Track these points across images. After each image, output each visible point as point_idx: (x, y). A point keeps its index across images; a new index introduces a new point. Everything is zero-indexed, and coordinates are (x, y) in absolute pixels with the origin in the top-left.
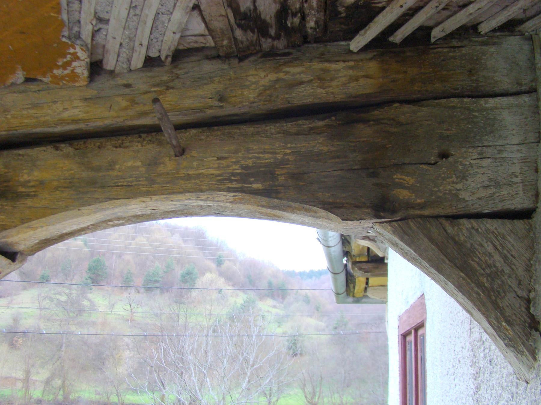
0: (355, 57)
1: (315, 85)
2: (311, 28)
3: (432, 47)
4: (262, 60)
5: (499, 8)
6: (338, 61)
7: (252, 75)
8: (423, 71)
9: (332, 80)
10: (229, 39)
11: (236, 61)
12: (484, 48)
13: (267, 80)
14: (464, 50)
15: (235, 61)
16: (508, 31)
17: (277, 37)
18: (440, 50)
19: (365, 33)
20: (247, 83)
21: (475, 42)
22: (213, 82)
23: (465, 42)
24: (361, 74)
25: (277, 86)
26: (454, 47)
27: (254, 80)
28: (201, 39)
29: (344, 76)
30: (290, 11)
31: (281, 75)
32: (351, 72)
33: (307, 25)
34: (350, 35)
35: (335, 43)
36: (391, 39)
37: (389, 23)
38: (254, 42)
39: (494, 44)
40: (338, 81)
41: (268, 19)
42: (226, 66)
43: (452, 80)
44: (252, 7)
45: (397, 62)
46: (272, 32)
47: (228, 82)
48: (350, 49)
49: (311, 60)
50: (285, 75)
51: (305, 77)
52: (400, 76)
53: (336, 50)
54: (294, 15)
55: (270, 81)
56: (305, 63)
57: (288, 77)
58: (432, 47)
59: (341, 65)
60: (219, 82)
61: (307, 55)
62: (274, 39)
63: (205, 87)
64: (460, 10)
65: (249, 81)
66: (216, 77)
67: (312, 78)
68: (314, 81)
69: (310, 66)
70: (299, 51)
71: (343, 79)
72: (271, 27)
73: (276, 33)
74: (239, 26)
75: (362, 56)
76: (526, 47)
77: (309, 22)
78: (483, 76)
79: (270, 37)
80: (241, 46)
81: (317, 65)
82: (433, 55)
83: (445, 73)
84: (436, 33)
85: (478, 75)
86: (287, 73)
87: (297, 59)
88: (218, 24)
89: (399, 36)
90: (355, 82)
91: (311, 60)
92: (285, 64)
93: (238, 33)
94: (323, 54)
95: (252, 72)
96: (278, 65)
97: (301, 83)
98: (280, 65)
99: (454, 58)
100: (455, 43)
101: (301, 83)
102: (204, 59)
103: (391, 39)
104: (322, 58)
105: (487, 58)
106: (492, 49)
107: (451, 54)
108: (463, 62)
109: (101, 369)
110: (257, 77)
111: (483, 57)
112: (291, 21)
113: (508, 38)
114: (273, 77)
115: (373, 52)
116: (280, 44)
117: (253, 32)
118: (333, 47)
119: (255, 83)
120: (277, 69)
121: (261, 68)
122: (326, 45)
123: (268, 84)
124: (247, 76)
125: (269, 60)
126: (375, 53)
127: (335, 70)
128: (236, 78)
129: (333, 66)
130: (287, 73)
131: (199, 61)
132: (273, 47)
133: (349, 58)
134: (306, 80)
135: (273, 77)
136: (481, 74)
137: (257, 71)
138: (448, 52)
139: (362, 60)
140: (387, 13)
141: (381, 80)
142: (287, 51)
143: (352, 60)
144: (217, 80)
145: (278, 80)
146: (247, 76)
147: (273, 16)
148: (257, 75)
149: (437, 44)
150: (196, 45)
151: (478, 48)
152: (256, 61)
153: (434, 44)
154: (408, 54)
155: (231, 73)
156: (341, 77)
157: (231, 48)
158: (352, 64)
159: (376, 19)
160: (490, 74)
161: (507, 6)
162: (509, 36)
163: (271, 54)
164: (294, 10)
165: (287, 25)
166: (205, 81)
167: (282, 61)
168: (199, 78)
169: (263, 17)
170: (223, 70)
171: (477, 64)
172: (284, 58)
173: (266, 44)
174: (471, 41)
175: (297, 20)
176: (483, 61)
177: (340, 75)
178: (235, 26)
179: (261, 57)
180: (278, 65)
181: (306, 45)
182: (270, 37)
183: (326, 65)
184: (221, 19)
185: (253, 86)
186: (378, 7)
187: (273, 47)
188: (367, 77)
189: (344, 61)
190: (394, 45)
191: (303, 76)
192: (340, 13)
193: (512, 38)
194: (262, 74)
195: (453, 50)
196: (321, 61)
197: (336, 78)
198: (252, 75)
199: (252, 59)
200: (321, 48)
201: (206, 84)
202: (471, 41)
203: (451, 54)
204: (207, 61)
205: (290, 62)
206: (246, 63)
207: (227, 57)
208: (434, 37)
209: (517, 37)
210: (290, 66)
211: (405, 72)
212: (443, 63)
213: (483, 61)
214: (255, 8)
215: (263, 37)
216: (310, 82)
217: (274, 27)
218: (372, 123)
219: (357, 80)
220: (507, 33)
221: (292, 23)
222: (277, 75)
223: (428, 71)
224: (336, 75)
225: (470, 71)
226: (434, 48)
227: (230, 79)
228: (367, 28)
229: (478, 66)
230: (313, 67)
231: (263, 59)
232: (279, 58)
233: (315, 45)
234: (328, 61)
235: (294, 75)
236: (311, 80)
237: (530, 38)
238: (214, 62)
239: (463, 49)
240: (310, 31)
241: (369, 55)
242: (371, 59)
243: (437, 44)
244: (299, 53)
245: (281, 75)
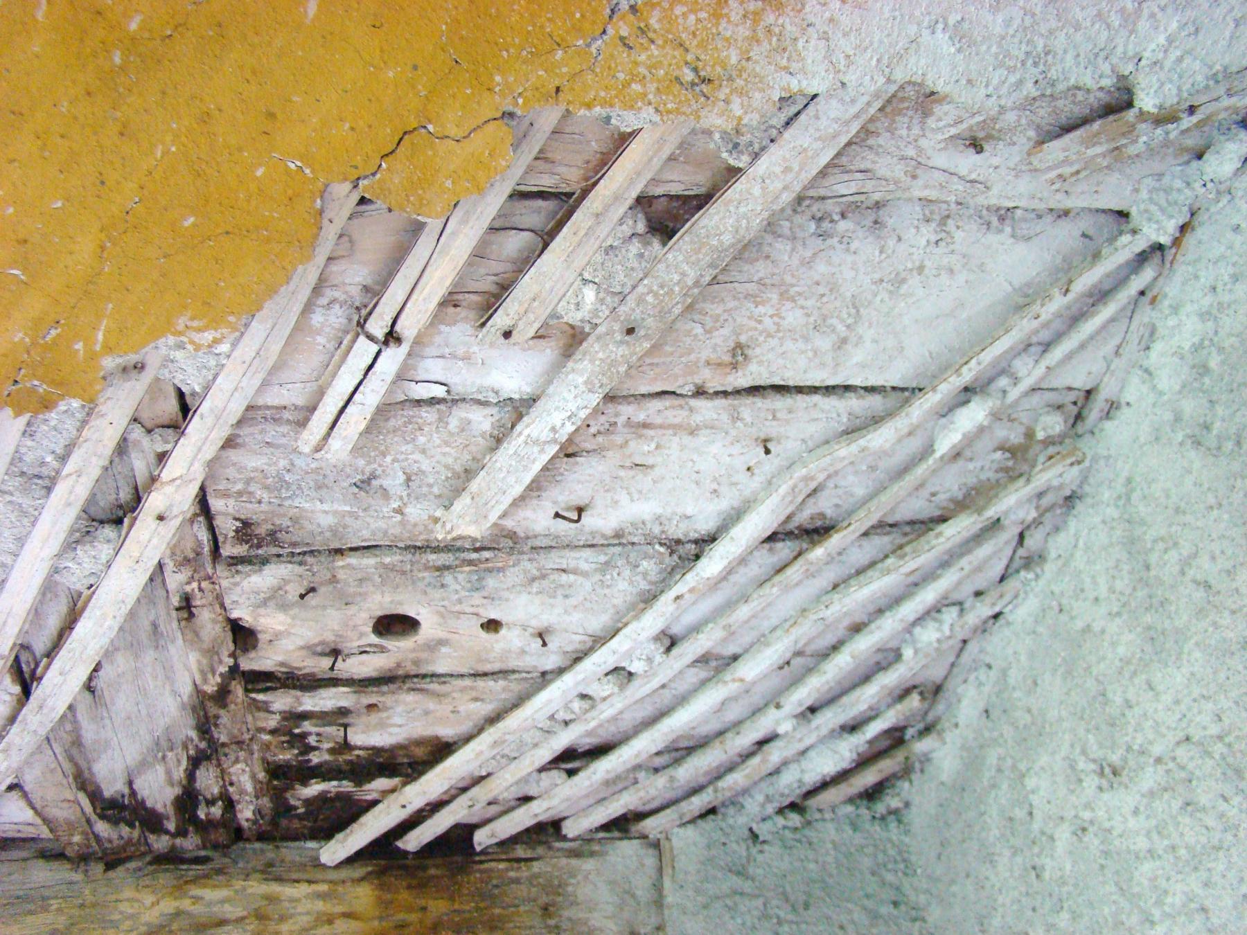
0: (334, 875)
1: (248, 928)
2: (247, 820)
3: (477, 858)
4: (151, 868)
5: (592, 801)
6: (297, 881)
7: (128, 900)
8: (456, 906)
9: (282, 919)
10: (84, 833)
11: (100, 867)
12: (574, 862)
13: (156, 912)
14: (536, 867)
15: (97, 869)
16: (620, 830)
17: (181, 832)
18: (493, 864)
19: (345, 839)
20: (116, 917)
21: (559, 850)
22: (45, 909)
23: (540, 850)
24: (340, 909)
25: (175, 927)
26: (518, 860)
27: (130, 911)
28: (31, 829)
29: (308, 913)
30: (201, 798)
31: (186, 904)
32: (320, 905)
33: (239, 816)
34: (327, 833)
35: (297, 844)
36: (400, 844)
37: (386, 829)
38: (135, 840)
39: (592, 854)
40: (295, 923)
41: (159, 808)
42: (78, 876)
43: (511, 925)
44: (126, 791)
45: (409, 887)
46: (171, 826)
47: (76, 912)
48: (318, 859)
49: (247, 877)
50: (194, 904)
51: (231, 911)
52: (413, 917)
53: (298, 858)
54: (211, 802)
55: (161, 915)
56: (234, 882)
57: (197, 909)
58: (477, 858)
59: (304, 889)
60: (59, 910)
61: (241, 865)
62: (174, 836)
63: (30, 919)
64: (519, 806)
65: (121, 913)
66: (56, 897)
67: (245, 913)
68: (247, 921)
69: (244, 889)
70: (225, 855)
71: (305, 918)
72: (168, 819)
73: (177, 827)
74: (102, 817)
75: (345, 873)
76: (650, 861)
77: (241, 811)
78: (570, 919)
79: (167, 832)
80: (107, 845)
81: (257, 887)
82: (478, 875)
83: (497, 911)
84: (481, 838)
85: (560, 916)
86: (197, 899)
87: (220, 871)
88: (60, 813)
89: (413, 841)
90: (327, 927)
91: (247, 875)
92: (194, 881)
93: (102, 828)
94: (271, 864)
95: (128, 893)
96: (181, 882)
97: (222, 923)
98: (186, 882)
99: (517, 881)
100: (520, 851)
101: (222, 923)
102: (36, 857)
103: (400, 844)
104: (269, 872)
105: (578, 883)
106: (589, 865)
107: (512, 874)
108: (534, 890)
109: (1196, 869)
110: (136, 905)
111: (573, 881)
112: (206, 810)
113: (618, 843)
114: (168, 906)
115: (367, 865)
116: (190, 843)
117: (131, 825)
118: (292, 852)
119: (131, 917)
120: (179, 889)
121: (147, 886)
122: (277, 847)
123: (156, 922)
124: (117, 901)
125: (167, 870)
126: (370, 869)
127: (292, 900)
128: (94, 905)
129: (288, 891)
130: (197, 899)
131: (25, 860)
132: (173, 848)
133: (319, 876)
134: (232, 917)
135: (168, 906)
136: (566, 913)
137: (138, 891)
138: (507, 870)
139: (344, 882)
140: (381, 812)
141: (376, 923)
142: (203, 853)
143: (323, 881)
144: (55, 904)
145: (178, 914)
146: (117, 901)
147: (168, 803)
148: (138, 901)
149: (488, 854)
150: (19, 835)
151: (564, 861)
152: (140, 869)
153: (483, 852)
154: (432, 871)
155: (87, 892)
156: (300, 914)
157: (88, 846)
158: (323, 887)
159: (363, 819)
160: (581, 915)
161: (604, 799)
162: (621, 839)
163: (171, 859)
164: (209, 797)
165: (198, 817)
166: (31, 907)
167: (191, 873)
168: (18, 898)
169: (149, 804)
170: (71, 883)
171: (559, 895)
172: (194, 867)
173: (160, 843)
174: (550, 848)
175: (217, 811)
176: (570, 889)
177: (300, 910)
178: (94, 817)
179: (150, 863)
180: (181, 882)
181: (241, 845)
182: (167, 832)
183: (275, 888)
184: (66, 805)
185: (127, 924)
186: (366, 801)
187: (173, 848)
188: (347, 915)
189: (310, 882)
190: (405, 853)
191: (227, 907)
192: (296, 808)
193: (625, 843)
194: (149, 899)
195: (515, 865)
196: (265, 879)
197: (291, 916)
198: (128, 900)
199: (132, 865)
200: (268, 851)
201: (31, 913)
202: (550, 848)
203: (512, 874)
204: (41, 862)
205: (206, 876)
206: (120, 871)
207: (83, 859)
208: (480, 844)
209: (635, 842)
210: (205, 886)
211: (424, 909)
212: (496, 891)
213: (570, 889)
214: (133, 793)
215: (153, 832)
216: (240, 920)
217: (173, 819)
218: (1106, 380)
219: (330, 922)
220: (616, 834)
221: (207, 815)
222: (176, 904)
223: (467, 908)
224: (292, 911)
225: (545, 908)
226: (481, 862)
227: (82, 906)
228: (348, 831)
229: (561, 899)
230: (250, 891)
231: (154, 867)
232: (185, 867)
233: (258, 845)
234: (279, 879)
235: (210, 904)
236: (243, 919)
237: (656, 845)
238: (55, 865)
239: (535, 863)
240: (245, 824)
241: (359, 871)
242: (362, 879)
243: (488, 854)
244: (227, 860)
245: (186, 904)
